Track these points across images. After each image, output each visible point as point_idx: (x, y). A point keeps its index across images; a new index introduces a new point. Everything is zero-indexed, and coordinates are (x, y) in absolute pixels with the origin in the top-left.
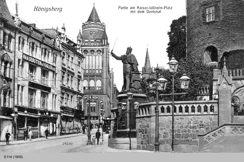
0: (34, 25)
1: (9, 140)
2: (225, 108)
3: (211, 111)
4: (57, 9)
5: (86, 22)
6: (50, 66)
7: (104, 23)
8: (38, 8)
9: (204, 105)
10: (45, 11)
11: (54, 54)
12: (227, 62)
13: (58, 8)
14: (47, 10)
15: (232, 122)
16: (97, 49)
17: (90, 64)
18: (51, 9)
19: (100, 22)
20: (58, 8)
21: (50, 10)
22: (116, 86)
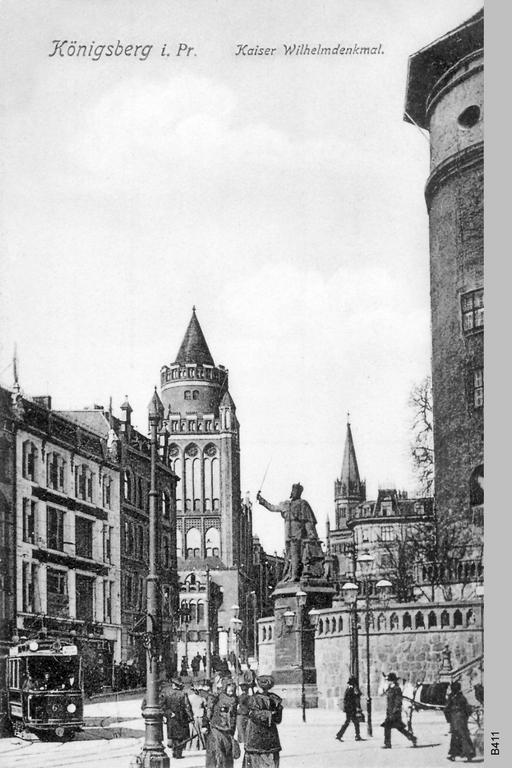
0: (46, 400)
4: (135, 48)
5: (172, 365)
7: (223, 367)
11: (104, 477)
13: (137, 48)
16: (207, 443)
17: (189, 495)
19: (213, 364)
20: (137, 48)
22: (260, 542)
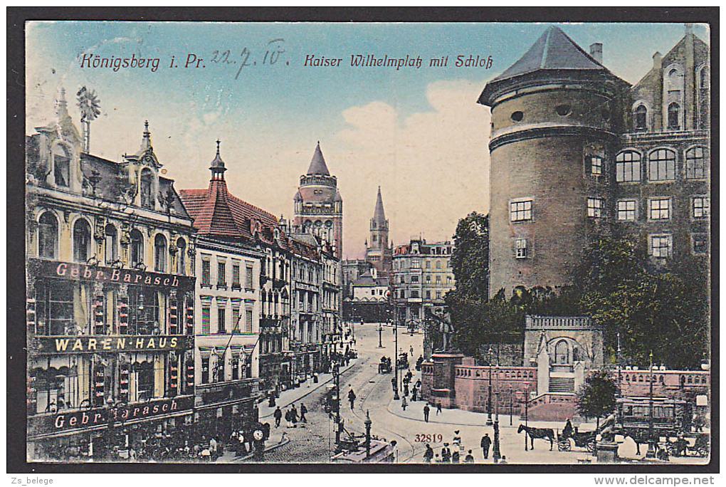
1: (513, 416)
2: (95, 182)
3: (689, 382)
4: (146, 61)
6: (224, 351)
8: (93, 58)
9: (660, 375)
10: (111, 66)
12: (520, 326)
14: (117, 64)
15: (156, 269)
18: (130, 62)
21: (126, 65)
